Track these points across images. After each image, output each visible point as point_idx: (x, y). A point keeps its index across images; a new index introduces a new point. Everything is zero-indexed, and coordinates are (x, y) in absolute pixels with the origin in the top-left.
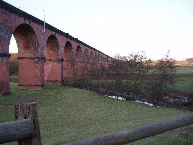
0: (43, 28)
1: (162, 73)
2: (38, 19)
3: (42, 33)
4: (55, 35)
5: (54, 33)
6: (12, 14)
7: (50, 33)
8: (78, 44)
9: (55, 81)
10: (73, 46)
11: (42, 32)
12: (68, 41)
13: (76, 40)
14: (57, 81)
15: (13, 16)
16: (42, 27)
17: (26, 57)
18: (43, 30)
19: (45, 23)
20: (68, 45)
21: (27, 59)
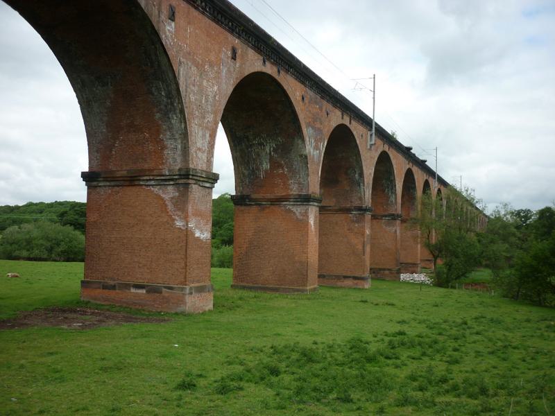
0: (371, 135)
1: (22, 225)
2: (363, 113)
3: (369, 147)
4: (348, 124)
5: (346, 121)
6: (325, 102)
7: (337, 118)
8: (337, 118)
9: (380, 269)
10: (416, 181)
11: (369, 143)
12: (340, 122)
13: (406, 152)
14: (384, 269)
15: (327, 106)
16: (369, 133)
17: (328, 205)
18: (371, 140)
19: (376, 124)
20: (341, 142)
21: (330, 210)
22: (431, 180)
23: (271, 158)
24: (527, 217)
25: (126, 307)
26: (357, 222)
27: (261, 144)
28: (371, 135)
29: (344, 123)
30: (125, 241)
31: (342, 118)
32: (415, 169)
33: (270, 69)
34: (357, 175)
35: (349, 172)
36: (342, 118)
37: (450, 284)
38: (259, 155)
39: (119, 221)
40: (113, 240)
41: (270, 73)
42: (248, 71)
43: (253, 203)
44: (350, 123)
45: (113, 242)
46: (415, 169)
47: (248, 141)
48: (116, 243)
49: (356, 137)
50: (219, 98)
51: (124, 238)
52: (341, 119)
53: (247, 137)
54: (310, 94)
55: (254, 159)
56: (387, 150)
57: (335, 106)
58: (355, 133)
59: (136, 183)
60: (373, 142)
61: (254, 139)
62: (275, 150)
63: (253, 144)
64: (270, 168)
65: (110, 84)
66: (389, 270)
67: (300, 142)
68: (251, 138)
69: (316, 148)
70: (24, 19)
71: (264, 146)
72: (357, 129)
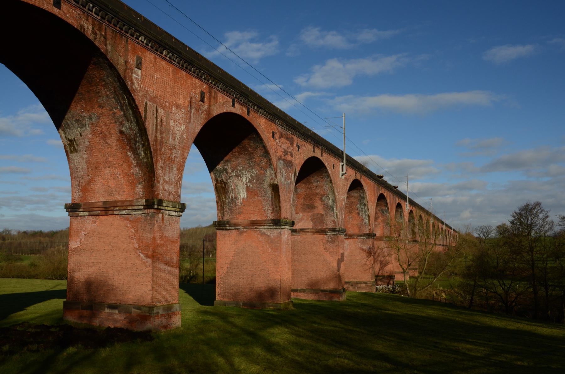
0: (343, 166)
4: (319, 157)
5: (318, 154)
9: (357, 283)
12: (311, 155)
14: (361, 283)
16: (341, 164)
17: (306, 228)
18: (343, 171)
22: (402, 203)
23: (248, 189)
24: (488, 233)
25: (265, 258)
26: (332, 242)
27: (238, 176)
28: (343, 166)
29: (315, 156)
30: (101, 266)
31: (314, 152)
32: (387, 194)
33: (238, 109)
34: (330, 201)
35: (324, 198)
36: (314, 152)
37: (379, 186)
38: (236, 186)
39: (96, 248)
40: (91, 265)
41: (240, 114)
42: (216, 112)
43: (233, 228)
44: (322, 156)
45: (91, 267)
46: (387, 194)
47: (227, 173)
48: (93, 268)
49: (328, 168)
50: (187, 136)
51: (100, 263)
52: (312, 152)
53: (226, 170)
54: (277, 128)
55: (233, 190)
56: (359, 178)
57: (306, 140)
58: (326, 164)
59: (110, 212)
60: (344, 172)
61: (232, 171)
62: (250, 181)
63: (232, 176)
64: (247, 197)
65: (87, 126)
66: (365, 283)
67: (327, 187)
68: (230, 170)
69: (287, 178)
70: (19, 79)
71: (241, 177)
72: (327, 160)
